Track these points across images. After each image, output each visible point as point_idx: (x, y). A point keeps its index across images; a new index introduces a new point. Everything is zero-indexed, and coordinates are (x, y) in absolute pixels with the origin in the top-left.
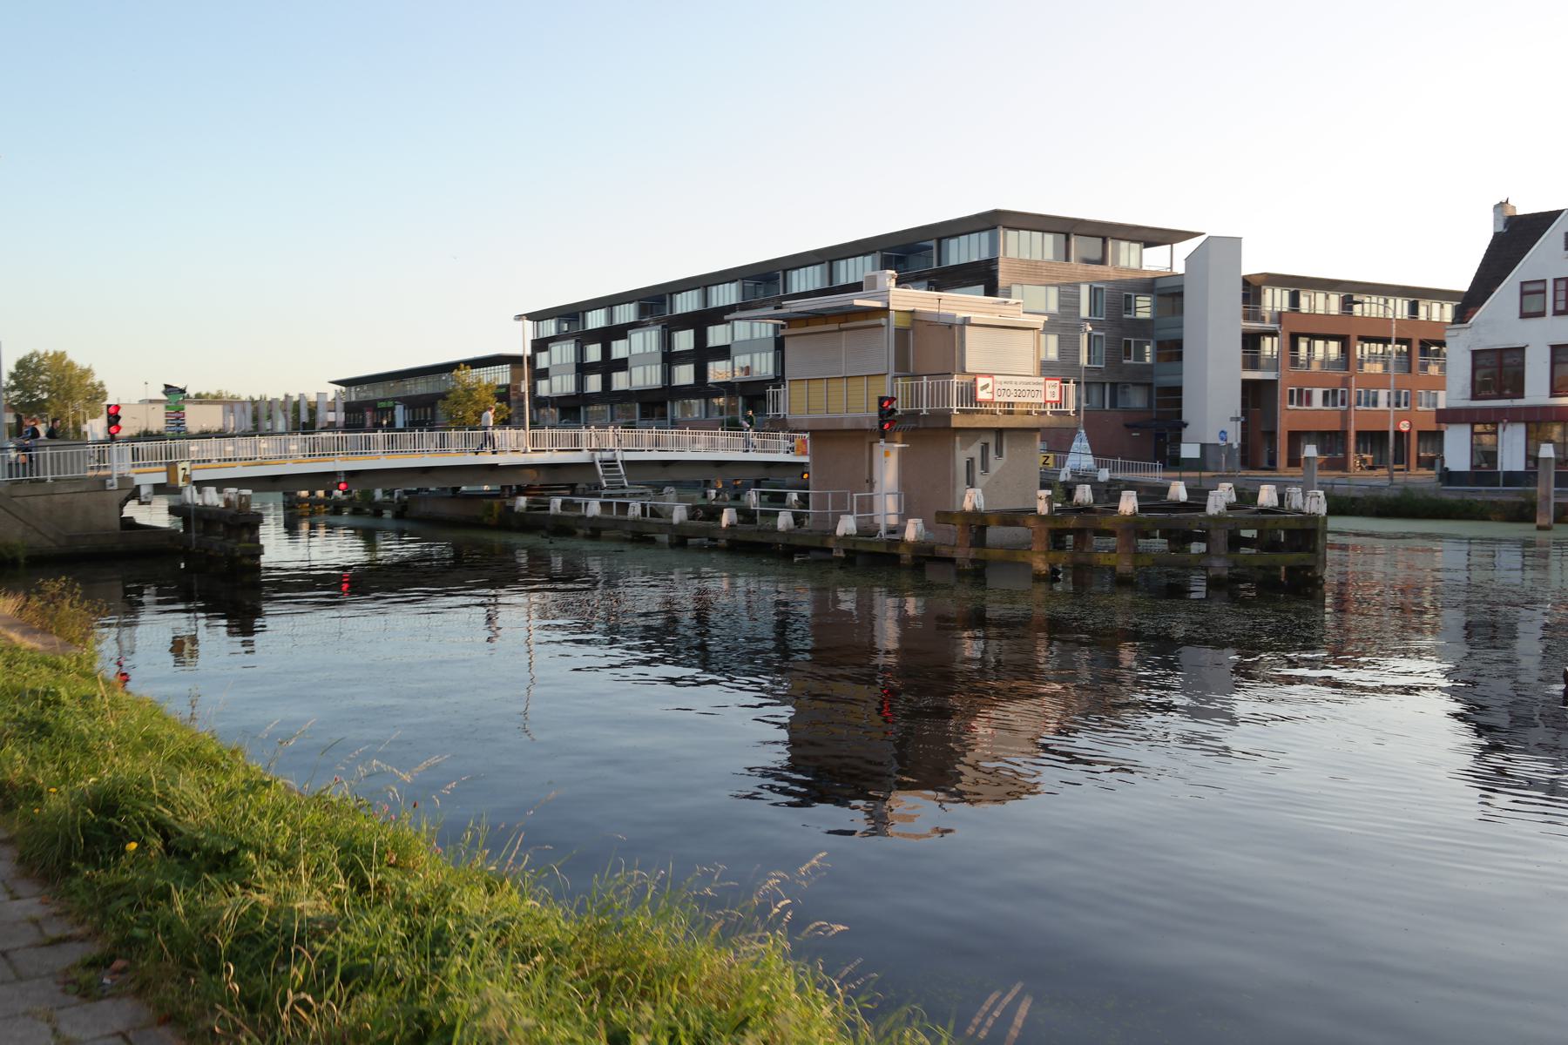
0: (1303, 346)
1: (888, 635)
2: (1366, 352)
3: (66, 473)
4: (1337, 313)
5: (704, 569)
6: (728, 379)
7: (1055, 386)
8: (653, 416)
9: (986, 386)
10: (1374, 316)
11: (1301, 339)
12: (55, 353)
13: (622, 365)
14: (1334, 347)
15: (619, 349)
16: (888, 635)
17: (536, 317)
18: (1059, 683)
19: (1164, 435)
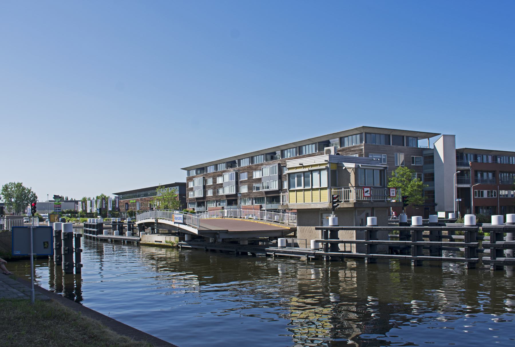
0: (479, 175)
1: (73, 293)
2: (502, 176)
3: (346, 191)
4: (491, 162)
5: (276, 259)
6: (223, 194)
7: (394, 191)
8: (232, 204)
9: (367, 191)
10: (505, 163)
11: (478, 172)
12: (18, 183)
13: (221, 186)
14: (490, 175)
15: (220, 180)
16: (73, 293)
17: (188, 169)
18: (469, 304)
19: (428, 209)
